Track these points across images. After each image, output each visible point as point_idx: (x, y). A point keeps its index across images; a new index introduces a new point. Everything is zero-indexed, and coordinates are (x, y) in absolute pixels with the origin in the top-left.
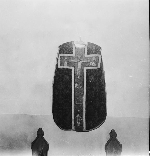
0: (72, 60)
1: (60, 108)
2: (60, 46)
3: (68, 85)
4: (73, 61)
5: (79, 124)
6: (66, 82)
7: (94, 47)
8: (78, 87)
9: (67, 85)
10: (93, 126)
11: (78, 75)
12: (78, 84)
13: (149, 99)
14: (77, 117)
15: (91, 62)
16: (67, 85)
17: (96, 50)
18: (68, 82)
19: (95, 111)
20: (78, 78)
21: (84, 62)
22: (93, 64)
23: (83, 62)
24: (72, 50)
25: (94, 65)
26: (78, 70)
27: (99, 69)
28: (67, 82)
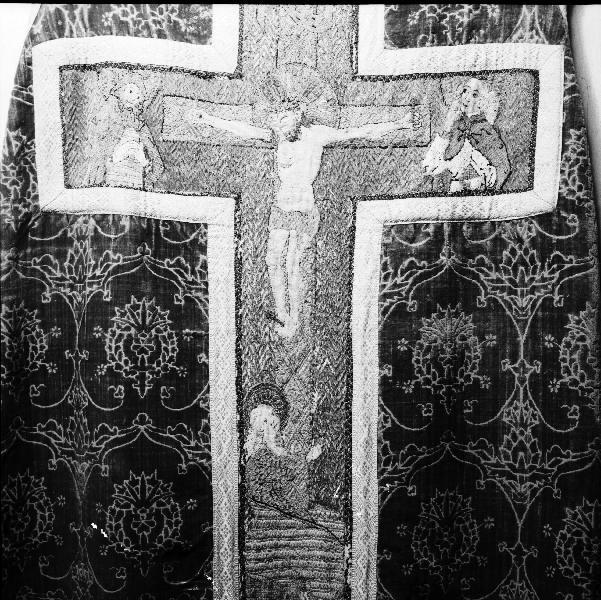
4: (219, 124)
6: (130, 393)
8: (279, 451)
11: (280, 303)
18: (157, 384)
23: (342, 136)
25: (470, 173)
26: (277, 236)
27: (544, 219)
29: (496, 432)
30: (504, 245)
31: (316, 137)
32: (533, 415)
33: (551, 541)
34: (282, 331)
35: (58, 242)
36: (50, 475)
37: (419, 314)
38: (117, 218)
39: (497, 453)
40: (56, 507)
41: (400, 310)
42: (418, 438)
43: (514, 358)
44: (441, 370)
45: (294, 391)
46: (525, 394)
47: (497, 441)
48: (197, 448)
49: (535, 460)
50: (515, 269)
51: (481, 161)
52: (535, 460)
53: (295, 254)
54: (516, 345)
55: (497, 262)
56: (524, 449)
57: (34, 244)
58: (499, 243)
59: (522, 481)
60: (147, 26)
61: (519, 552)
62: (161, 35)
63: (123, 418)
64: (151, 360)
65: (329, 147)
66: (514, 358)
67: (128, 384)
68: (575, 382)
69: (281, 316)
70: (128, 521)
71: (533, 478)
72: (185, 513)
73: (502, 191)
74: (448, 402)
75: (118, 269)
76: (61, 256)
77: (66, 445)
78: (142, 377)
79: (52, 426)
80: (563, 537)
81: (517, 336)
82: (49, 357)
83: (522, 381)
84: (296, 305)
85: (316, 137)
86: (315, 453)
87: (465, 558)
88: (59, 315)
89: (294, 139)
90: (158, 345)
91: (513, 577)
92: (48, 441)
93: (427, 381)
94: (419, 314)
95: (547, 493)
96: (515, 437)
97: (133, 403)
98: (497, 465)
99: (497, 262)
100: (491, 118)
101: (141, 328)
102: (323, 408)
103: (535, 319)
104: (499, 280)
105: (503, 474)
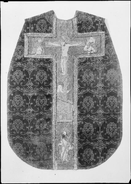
0: (51, 44)
1: (27, 128)
2: (26, 20)
3: (92, 117)
4: (54, 44)
5: (64, 157)
6: (40, 83)
7: (90, 19)
8: (62, 92)
9: (88, 116)
10: (95, 160)
11: (62, 69)
12: (63, 85)
13: (107, 183)
14: (61, 144)
15: (86, 47)
16: (88, 116)
17: (94, 25)
18: (44, 82)
19: (98, 132)
20: (64, 74)
21: (73, 47)
22: (89, 50)
23: (71, 45)
24: (51, 26)
25: (92, 51)
26: (62, 60)
27: (103, 57)
28: (43, 83)
29: (96, 89)
30: (97, 61)
31: (68, 46)
32: (102, 85)
33: (106, 103)
34: (63, 74)
35: (26, 62)
36: (23, 96)
37: (83, 71)
38: (38, 59)
39: (96, 91)
40: (36, 99)
41: (81, 71)
42: (13, 87)
43: (99, 77)
44: (87, 79)
45: (65, 83)
46: (101, 82)
47: (96, 90)
48: (50, 91)
49: (102, 92)
50: (99, 64)
51: (93, 49)
52: (102, 92)
53: (65, 62)
54: (99, 75)
55: (96, 63)
56: (101, 90)
57: (23, 62)
58: (97, 61)
59: (100, 95)
60: (42, 31)
61: (100, 106)
62: (44, 32)
63: (39, 87)
64: (43, 79)
65: (70, 47)
66: (99, 77)
67: (39, 82)
68: (109, 80)
69: (62, 72)
70: (39, 101)
71: (102, 95)
72: (48, 100)
73: (97, 53)
74: (88, 84)
75: (38, 66)
76: (26, 64)
77: (50, 91)
78: (41, 81)
79: (47, 89)
80: (107, 102)
81: (99, 74)
82: (23, 79)
83: (100, 80)
84: (65, 69)
85: (68, 46)
86: (68, 92)
87: (92, 107)
88: (26, 73)
89: (64, 46)
90: (44, 77)
91: (99, 109)
92: (23, 91)
93: (85, 81)
94: (83, 71)
95: (105, 148)
96: (99, 89)
97: (40, 85)
98: (97, 93)
99: (96, 63)
100: (94, 43)
101: (41, 74)
102: (69, 85)
103: (102, 71)
104: (96, 66)
105: (98, 94)
